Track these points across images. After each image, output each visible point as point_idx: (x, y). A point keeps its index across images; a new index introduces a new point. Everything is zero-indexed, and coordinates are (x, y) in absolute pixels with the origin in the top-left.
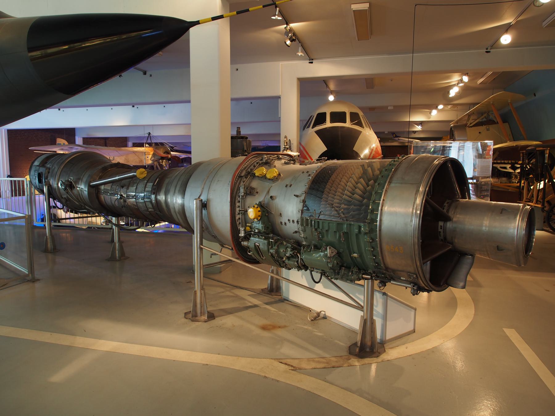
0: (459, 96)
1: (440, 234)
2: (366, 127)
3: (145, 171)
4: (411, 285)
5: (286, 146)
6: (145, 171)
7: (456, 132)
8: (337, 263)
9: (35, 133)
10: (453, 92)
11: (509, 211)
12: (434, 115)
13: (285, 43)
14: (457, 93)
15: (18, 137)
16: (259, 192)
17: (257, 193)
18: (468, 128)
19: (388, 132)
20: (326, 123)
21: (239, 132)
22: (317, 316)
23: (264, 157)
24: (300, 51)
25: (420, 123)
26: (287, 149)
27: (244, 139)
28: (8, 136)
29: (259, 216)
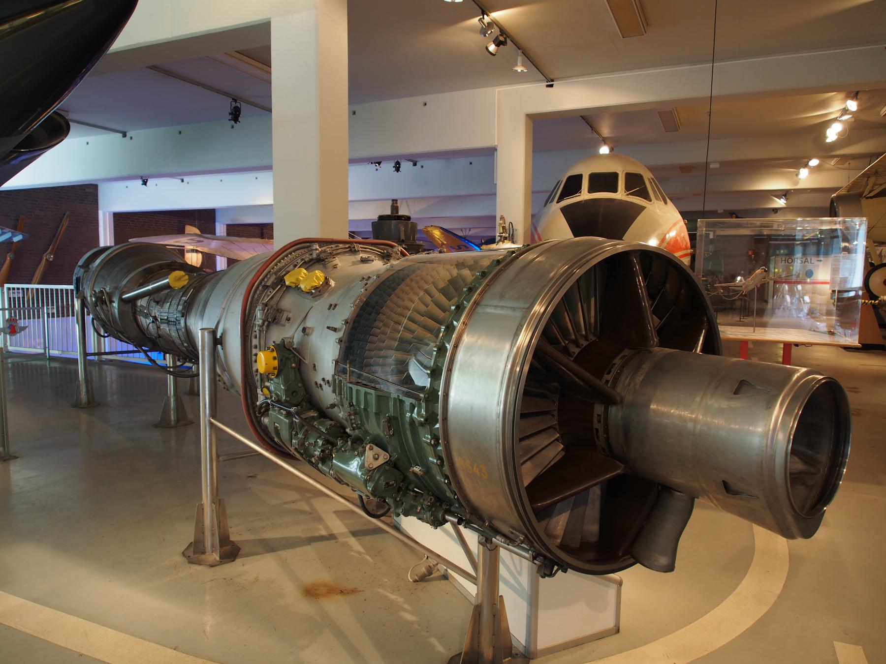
0: (845, 139)
1: (597, 435)
2: (657, 198)
3: (183, 276)
4: (528, 553)
5: (502, 233)
6: (183, 276)
7: (840, 208)
8: (387, 483)
9: (154, 218)
10: (833, 134)
11: (758, 387)
12: (805, 178)
13: (487, 48)
14: (840, 134)
15: (129, 223)
16: (292, 319)
17: (288, 319)
18: (864, 199)
19: (724, 211)
20: (580, 192)
21: (395, 208)
22: (426, 573)
23: (314, 248)
24: (519, 63)
25: (784, 194)
26: (505, 238)
27: (403, 220)
28: (114, 222)
29: (275, 368)
